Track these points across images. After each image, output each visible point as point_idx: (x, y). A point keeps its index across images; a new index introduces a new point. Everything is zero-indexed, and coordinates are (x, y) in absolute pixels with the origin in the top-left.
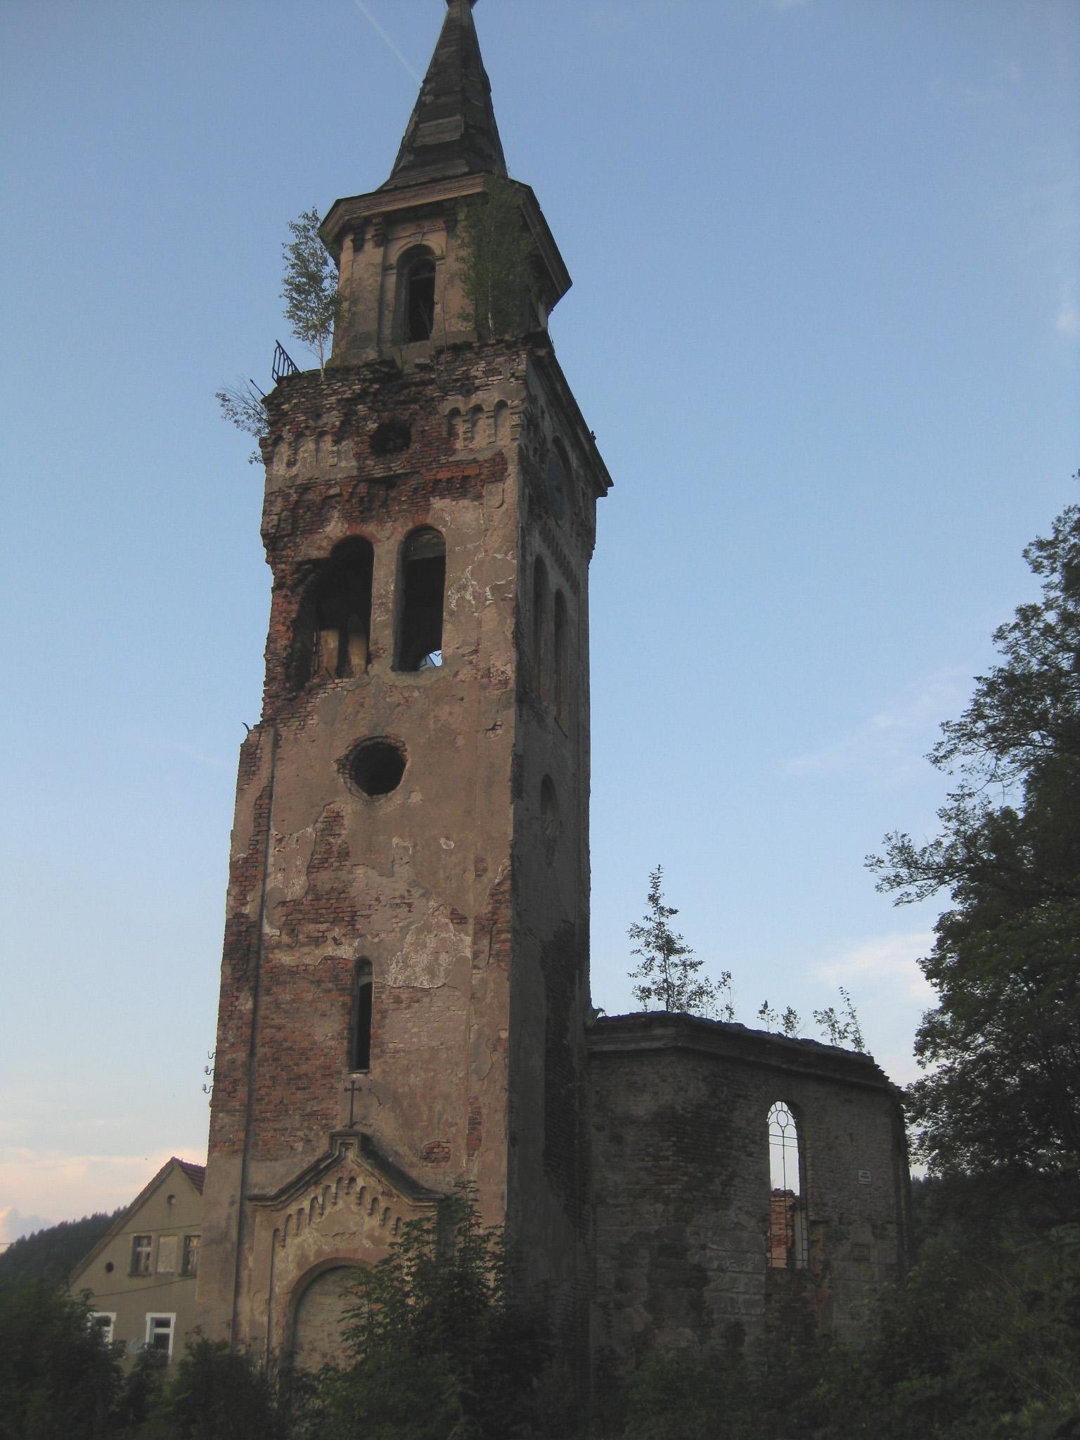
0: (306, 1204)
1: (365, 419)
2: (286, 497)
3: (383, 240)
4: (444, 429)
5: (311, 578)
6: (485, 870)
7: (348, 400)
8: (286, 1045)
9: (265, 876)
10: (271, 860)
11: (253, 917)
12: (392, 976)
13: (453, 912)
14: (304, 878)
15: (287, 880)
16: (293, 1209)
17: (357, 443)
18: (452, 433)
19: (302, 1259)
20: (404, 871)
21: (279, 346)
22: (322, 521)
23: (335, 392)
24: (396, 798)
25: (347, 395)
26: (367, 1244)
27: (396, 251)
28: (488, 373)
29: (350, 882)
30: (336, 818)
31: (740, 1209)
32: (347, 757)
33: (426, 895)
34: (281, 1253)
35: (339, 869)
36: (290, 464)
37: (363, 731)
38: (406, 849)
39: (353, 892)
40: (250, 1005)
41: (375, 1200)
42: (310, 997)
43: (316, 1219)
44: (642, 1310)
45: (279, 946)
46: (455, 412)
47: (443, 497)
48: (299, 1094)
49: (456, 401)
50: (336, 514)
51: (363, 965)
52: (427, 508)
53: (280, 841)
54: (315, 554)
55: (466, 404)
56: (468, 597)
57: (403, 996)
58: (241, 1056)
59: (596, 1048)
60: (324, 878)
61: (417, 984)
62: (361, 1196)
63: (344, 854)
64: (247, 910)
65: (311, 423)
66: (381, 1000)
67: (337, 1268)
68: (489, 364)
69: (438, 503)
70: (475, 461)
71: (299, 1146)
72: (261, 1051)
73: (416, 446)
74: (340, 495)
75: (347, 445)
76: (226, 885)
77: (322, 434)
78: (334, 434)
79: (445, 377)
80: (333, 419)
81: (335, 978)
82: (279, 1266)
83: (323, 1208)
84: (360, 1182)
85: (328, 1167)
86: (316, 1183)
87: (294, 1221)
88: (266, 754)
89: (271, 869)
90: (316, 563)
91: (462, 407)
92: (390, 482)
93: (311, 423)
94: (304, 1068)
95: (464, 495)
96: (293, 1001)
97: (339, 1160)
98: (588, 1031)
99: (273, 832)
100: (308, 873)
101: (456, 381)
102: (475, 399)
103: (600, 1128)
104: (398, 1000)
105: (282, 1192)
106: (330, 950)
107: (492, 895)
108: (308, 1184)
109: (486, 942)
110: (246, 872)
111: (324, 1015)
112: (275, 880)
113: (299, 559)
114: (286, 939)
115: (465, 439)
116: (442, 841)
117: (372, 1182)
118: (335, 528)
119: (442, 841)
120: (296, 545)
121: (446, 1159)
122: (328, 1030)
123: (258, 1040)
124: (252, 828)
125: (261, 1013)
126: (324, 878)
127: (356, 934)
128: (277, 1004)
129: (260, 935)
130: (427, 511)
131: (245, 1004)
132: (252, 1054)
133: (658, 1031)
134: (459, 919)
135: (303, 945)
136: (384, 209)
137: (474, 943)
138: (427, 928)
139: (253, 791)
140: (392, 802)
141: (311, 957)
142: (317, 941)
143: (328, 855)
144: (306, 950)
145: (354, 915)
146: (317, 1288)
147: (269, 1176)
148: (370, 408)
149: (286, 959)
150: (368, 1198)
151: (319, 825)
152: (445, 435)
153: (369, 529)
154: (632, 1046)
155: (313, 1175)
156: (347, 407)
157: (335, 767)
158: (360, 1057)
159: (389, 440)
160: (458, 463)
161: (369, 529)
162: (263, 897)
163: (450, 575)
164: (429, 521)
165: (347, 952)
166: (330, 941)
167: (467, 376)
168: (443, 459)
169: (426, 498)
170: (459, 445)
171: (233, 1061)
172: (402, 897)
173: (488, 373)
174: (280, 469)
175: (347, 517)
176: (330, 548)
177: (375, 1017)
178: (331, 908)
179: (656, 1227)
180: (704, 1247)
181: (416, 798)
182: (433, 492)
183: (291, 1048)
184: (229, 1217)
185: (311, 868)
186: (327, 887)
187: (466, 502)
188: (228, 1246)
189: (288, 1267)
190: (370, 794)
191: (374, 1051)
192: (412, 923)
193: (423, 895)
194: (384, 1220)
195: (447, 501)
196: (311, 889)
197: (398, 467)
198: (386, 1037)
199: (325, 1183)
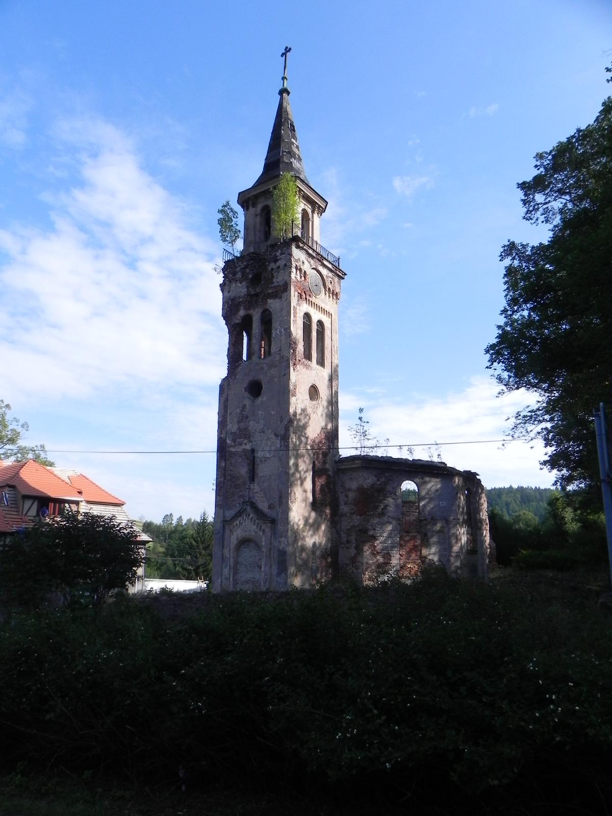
0: (238, 523)
1: (249, 274)
2: (228, 303)
3: (254, 205)
4: (270, 275)
5: (237, 329)
6: (283, 420)
7: (243, 268)
8: (234, 475)
9: (227, 425)
10: (228, 420)
11: (224, 438)
12: (259, 454)
13: (275, 433)
14: (237, 425)
15: (233, 427)
16: (235, 524)
17: (246, 283)
18: (273, 277)
19: (237, 538)
20: (262, 422)
21: (225, 250)
22: (238, 310)
23: (239, 266)
24: (260, 399)
25: (243, 267)
26: (253, 534)
27: (260, 207)
28: (282, 254)
29: (249, 425)
30: (244, 407)
31: (389, 517)
32: (247, 387)
33: (268, 429)
34: (232, 537)
35: (245, 422)
36: (229, 292)
37: (251, 379)
38: (262, 415)
39: (249, 428)
40: (224, 465)
41: (255, 521)
42: (239, 461)
43: (241, 526)
44: (354, 549)
45: (231, 446)
46: (272, 269)
47: (271, 299)
48: (238, 490)
49: (272, 265)
50: (242, 307)
51: (253, 451)
52: (266, 303)
53: (230, 414)
54: (237, 321)
55: (275, 265)
56: (278, 332)
57: (263, 460)
58: (222, 479)
59: (339, 468)
60: (242, 425)
61: (266, 456)
62: (251, 519)
63: (247, 417)
64: (222, 436)
65: (233, 278)
66: (257, 461)
67: (247, 541)
68: (281, 250)
69: (269, 301)
70: (279, 285)
71: (238, 505)
72: (227, 477)
73: (263, 282)
74: (242, 301)
75: (244, 283)
76: (217, 429)
77: (236, 281)
78: (240, 280)
79: (269, 257)
80: (239, 275)
81: (245, 455)
82: (232, 540)
83: (242, 523)
84: (251, 516)
85: (243, 512)
86: (241, 516)
87: (235, 528)
88: (226, 388)
89: (228, 423)
90: (238, 324)
91: (274, 267)
92: (257, 295)
93: (233, 278)
94: (239, 482)
95: (276, 298)
96: (235, 462)
97: (245, 509)
98: (336, 462)
99: (229, 412)
100: (238, 424)
101: (272, 258)
102: (278, 264)
103: (342, 493)
104: (261, 461)
105: (231, 519)
106: (244, 447)
107: (285, 428)
108: (238, 516)
109: (283, 442)
110: (222, 424)
111: (243, 466)
112: (229, 426)
113: (232, 324)
114: (233, 444)
115: (276, 278)
116: (272, 412)
117: (254, 515)
118: (242, 313)
119: (272, 412)
120: (232, 319)
121: (274, 508)
122: (244, 471)
123: (227, 475)
124: (223, 411)
125: (227, 466)
126: (242, 425)
127: (250, 441)
128: (231, 463)
129: (226, 443)
130: (266, 304)
131: (223, 464)
132: (225, 479)
133: (356, 462)
134: (276, 435)
135: (238, 445)
136: (254, 194)
137: (280, 442)
138: (268, 439)
139: (223, 399)
140: (259, 400)
141: (239, 449)
142: (241, 444)
143: (243, 418)
144: (238, 447)
145: (250, 435)
146: (242, 546)
147: (230, 514)
148: (250, 270)
149: (233, 450)
150: (253, 520)
151: (240, 409)
152: (270, 277)
153: (251, 312)
154: (350, 467)
155: (239, 514)
156: (243, 270)
157: (244, 390)
158: (252, 478)
159: (256, 280)
160: (274, 287)
161: (251, 312)
162: (226, 432)
163: (273, 325)
164: (267, 308)
165: (248, 447)
166: (244, 444)
167: (276, 256)
168: (270, 286)
169: (266, 299)
170: (274, 280)
171: (220, 481)
172: (262, 430)
173: (282, 254)
174: (226, 294)
175: (245, 309)
176: (240, 319)
177: (256, 466)
178: (244, 434)
179: (357, 524)
180: (374, 529)
181: (265, 399)
182: (268, 298)
183: (235, 477)
184: (220, 527)
185: (239, 422)
186: (243, 428)
187: (277, 300)
188: (220, 535)
189: (234, 540)
190: (254, 397)
191: (256, 477)
192: (264, 437)
193: (267, 429)
194: (257, 526)
195: (272, 300)
196: (239, 429)
197: (258, 290)
198: (258, 472)
199: (243, 516)
